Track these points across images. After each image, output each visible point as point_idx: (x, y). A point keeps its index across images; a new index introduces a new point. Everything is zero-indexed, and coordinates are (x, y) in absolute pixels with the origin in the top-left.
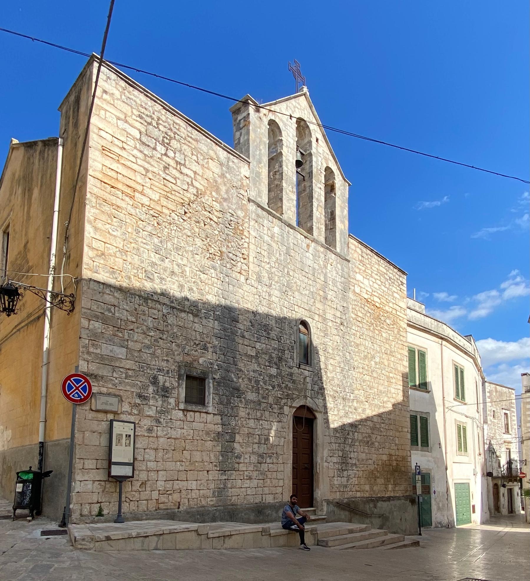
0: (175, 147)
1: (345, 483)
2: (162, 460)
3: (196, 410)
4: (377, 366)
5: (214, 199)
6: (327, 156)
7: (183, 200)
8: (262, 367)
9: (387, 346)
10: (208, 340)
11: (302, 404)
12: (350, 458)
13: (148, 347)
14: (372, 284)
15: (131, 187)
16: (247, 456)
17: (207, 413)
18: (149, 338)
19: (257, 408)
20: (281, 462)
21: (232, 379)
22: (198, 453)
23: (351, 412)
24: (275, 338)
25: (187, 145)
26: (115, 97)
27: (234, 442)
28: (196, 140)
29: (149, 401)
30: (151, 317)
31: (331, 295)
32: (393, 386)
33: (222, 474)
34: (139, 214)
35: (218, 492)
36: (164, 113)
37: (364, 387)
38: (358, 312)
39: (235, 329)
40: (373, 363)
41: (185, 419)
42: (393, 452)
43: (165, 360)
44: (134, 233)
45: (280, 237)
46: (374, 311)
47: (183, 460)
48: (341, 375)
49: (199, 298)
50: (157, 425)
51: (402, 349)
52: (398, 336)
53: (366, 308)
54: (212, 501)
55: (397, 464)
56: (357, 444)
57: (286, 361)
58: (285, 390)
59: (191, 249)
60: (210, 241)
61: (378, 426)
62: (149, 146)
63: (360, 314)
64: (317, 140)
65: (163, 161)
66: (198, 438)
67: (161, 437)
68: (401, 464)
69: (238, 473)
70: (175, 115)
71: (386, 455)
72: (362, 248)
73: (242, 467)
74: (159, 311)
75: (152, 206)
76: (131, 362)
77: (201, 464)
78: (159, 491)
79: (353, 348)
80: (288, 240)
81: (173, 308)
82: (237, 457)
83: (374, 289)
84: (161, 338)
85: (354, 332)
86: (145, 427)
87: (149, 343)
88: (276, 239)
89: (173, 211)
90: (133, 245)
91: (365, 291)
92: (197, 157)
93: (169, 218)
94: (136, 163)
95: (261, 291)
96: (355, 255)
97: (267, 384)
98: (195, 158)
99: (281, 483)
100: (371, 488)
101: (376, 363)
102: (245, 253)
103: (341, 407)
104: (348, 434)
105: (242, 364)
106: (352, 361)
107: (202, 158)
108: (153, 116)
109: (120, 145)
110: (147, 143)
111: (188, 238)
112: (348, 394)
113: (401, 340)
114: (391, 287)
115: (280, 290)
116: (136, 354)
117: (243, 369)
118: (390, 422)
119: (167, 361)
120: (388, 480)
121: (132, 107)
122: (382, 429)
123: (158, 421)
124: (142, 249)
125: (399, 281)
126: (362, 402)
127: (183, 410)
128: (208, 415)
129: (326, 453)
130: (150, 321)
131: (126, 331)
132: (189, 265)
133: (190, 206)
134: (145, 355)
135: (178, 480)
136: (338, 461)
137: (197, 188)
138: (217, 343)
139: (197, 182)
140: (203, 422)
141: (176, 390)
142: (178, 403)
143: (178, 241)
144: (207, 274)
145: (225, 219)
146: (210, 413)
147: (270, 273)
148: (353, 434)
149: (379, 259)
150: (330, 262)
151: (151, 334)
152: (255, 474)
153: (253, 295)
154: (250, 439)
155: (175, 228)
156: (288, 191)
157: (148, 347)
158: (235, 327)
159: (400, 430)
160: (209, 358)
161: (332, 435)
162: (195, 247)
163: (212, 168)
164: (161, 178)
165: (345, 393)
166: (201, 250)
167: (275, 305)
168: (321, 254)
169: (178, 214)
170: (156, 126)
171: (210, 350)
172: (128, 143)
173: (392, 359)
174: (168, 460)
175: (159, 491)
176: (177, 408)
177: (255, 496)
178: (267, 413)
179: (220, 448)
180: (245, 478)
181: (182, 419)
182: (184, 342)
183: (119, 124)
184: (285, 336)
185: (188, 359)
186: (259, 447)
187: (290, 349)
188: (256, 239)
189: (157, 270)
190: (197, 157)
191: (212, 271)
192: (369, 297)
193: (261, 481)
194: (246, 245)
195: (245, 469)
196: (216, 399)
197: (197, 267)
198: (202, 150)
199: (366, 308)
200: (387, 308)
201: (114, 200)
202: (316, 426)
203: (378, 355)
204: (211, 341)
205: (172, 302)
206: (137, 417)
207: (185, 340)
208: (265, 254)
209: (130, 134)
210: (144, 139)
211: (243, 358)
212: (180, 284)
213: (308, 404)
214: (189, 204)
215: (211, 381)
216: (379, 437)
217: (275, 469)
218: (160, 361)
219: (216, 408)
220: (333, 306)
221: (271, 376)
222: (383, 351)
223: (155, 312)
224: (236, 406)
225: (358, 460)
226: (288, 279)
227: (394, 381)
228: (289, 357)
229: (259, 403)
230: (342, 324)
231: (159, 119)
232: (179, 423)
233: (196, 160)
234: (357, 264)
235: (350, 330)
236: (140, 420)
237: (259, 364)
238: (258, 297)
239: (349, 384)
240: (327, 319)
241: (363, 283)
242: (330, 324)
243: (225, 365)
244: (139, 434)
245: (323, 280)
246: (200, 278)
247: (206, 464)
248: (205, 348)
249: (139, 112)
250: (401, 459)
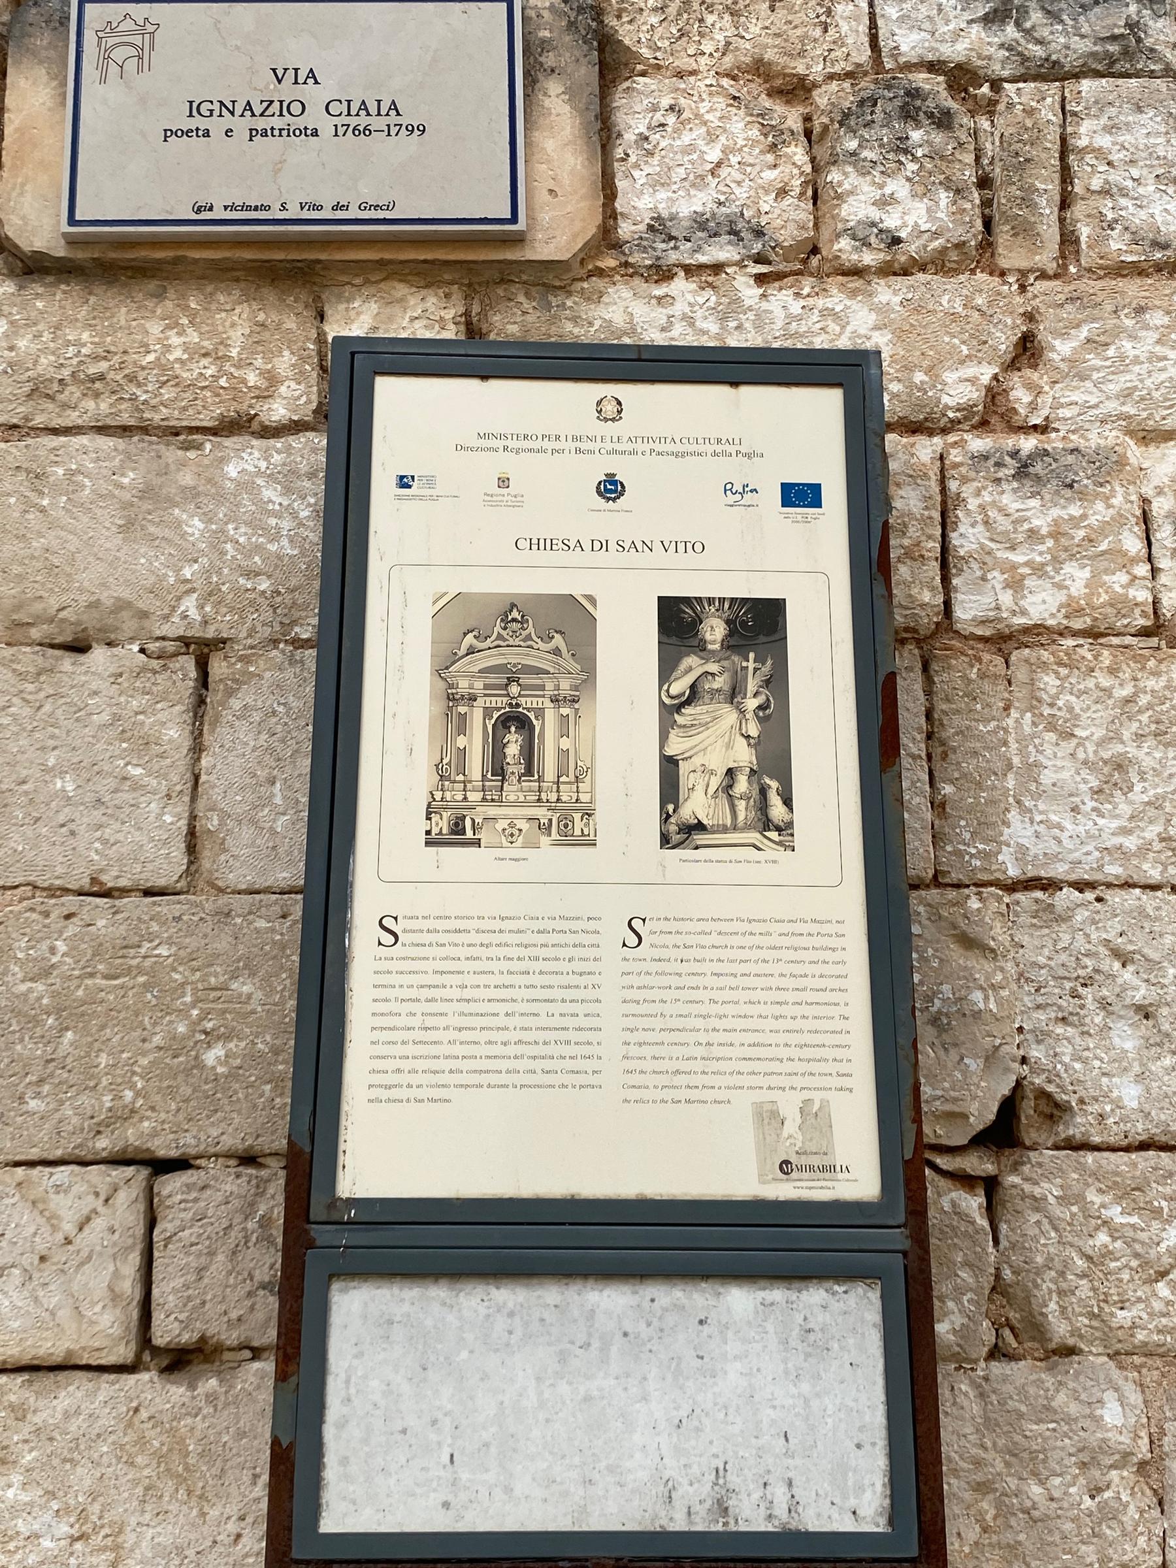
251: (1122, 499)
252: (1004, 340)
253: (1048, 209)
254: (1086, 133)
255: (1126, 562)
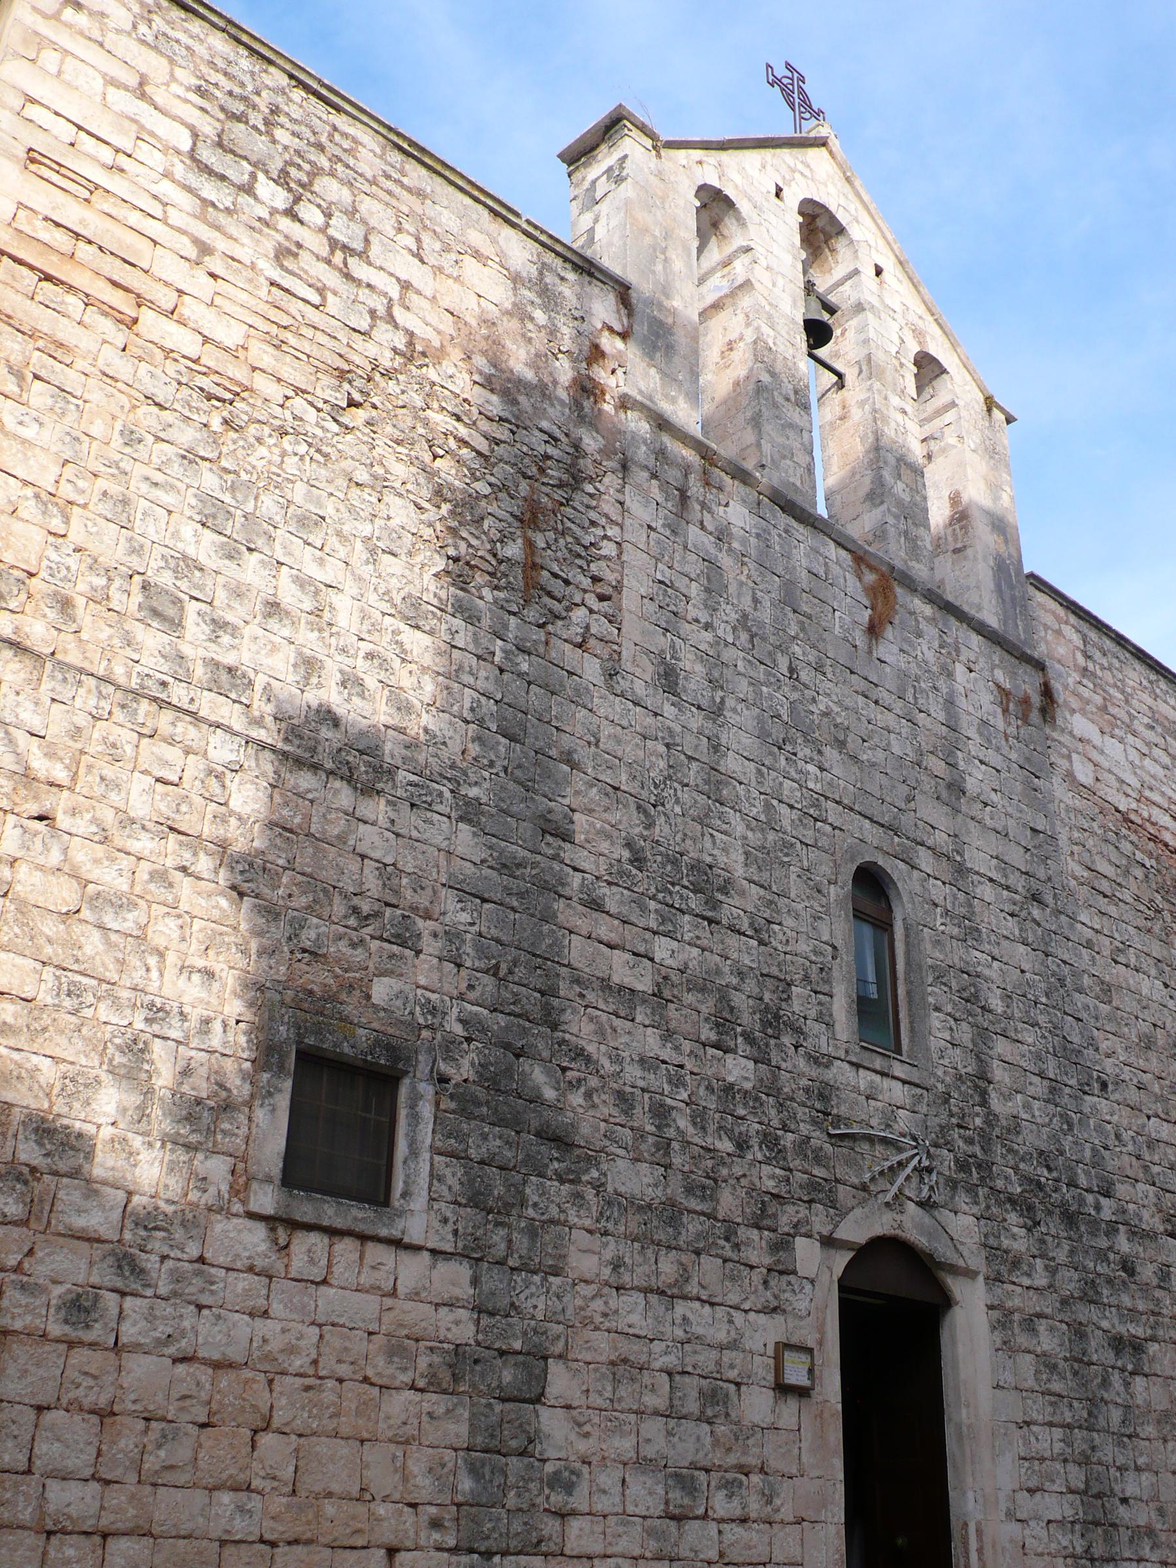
2: (132, 1478)
3: (339, 1223)
6: (920, 323)
8: (687, 1046)
10: (423, 900)
11: (878, 1231)
12: (1124, 1501)
15: (127, 290)
16: (608, 1479)
17: (397, 1244)
18: (126, 862)
19: (660, 1236)
20: (787, 1513)
21: (537, 1088)
22: (345, 1450)
23: (1110, 1281)
24: (745, 926)
25: (380, 200)
26: (112, 25)
27: (538, 1399)
28: (419, 194)
30: (145, 772)
31: (976, 780)
36: (298, 100)
37: (1156, 1169)
39: (556, 866)
41: (280, 1266)
45: (753, 540)
47: (256, 1483)
49: (391, 722)
50: (119, 1284)
53: (1126, 847)
56: (1150, 1430)
57: (799, 1031)
58: (796, 1163)
59: (366, 529)
62: (223, 178)
63: (1103, 867)
64: (879, 272)
65: (277, 231)
66: (344, 1370)
67: (136, 1348)
70: (338, 109)
72: (1085, 627)
74: (187, 752)
76: (19, 960)
77: (360, 1509)
79: (1091, 1002)
80: (787, 556)
83: (1147, 778)
84: (184, 869)
85: (1089, 933)
86: (58, 1290)
87: (123, 885)
89: (300, 391)
90: (101, 484)
92: (418, 240)
93: (278, 411)
94: (164, 221)
95: (678, 729)
96: (1061, 651)
97: (712, 1128)
102: (611, 577)
103: (1062, 1256)
104: (1105, 1383)
106: (1091, 1051)
107: (437, 246)
108: (256, 99)
109: (106, 155)
112: (1090, 1198)
115: (763, 735)
116: (50, 927)
117: (591, 1048)
119: (209, 974)
121: (172, 61)
124: (143, 503)
126: (1151, 1236)
128: (405, 1257)
131: (11, 819)
132: (351, 587)
136: (1069, 1512)
138: (465, 917)
140: (374, 1289)
141: (242, 1118)
142: (247, 1185)
143: (308, 497)
145: (525, 449)
146: (417, 1248)
147: (712, 660)
148: (1127, 1385)
149: (1153, 677)
153: (638, 740)
155: (302, 448)
158: (555, 857)
160: (422, 981)
161: (1031, 1383)
162: (386, 528)
164: (262, 279)
166: (408, 539)
167: (741, 789)
168: (923, 625)
169: (320, 405)
170: (263, 128)
171: (430, 946)
174: (168, 1477)
176: (237, 1207)
178: (710, 1264)
179: (464, 1429)
181: (259, 1263)
182: (303, 901)
183: (108, 97)
184: (789, 922)
185: (318, 978)
186: (670, 1433)
187: (814, 976)
189: (201, 588)
190: (418, 240)
192: (1134, 805)
194: (609, 549)
196: (450, 1180)
198: (440, 225)
199: (1126, 847)
201: (44, 320)
202: (954, 1342)
206: (16, 1232)
208: (694, 590)
210: (207, 155)
211: (591, 997)
212: (300, 654)
215: (427, 1090)
218: (170, 972)
219: (445, 1221)
223: (173, 754)
224: (552, 1221)
229: (672, 1213)
230: (1036, 898)
231: (275, 110)
232: (244, 1282)
233: (415, 249)
235: (1072, 927)
236: (31, 1252)
237: (668, 1035)
238: (662, 749)
240: (969, 870)
241: (1102, 752)
242: (986, 892)
243: (502, 1020)
244: (18, 1325)
245: (942, 717)
247: (381, 1510)
248: (405, 939)
249: (199, 78)
251: (44, 1298)
252: (26, 1250)
253: (46, 1215)
254: (61, 1194)
255: (40, 1315)
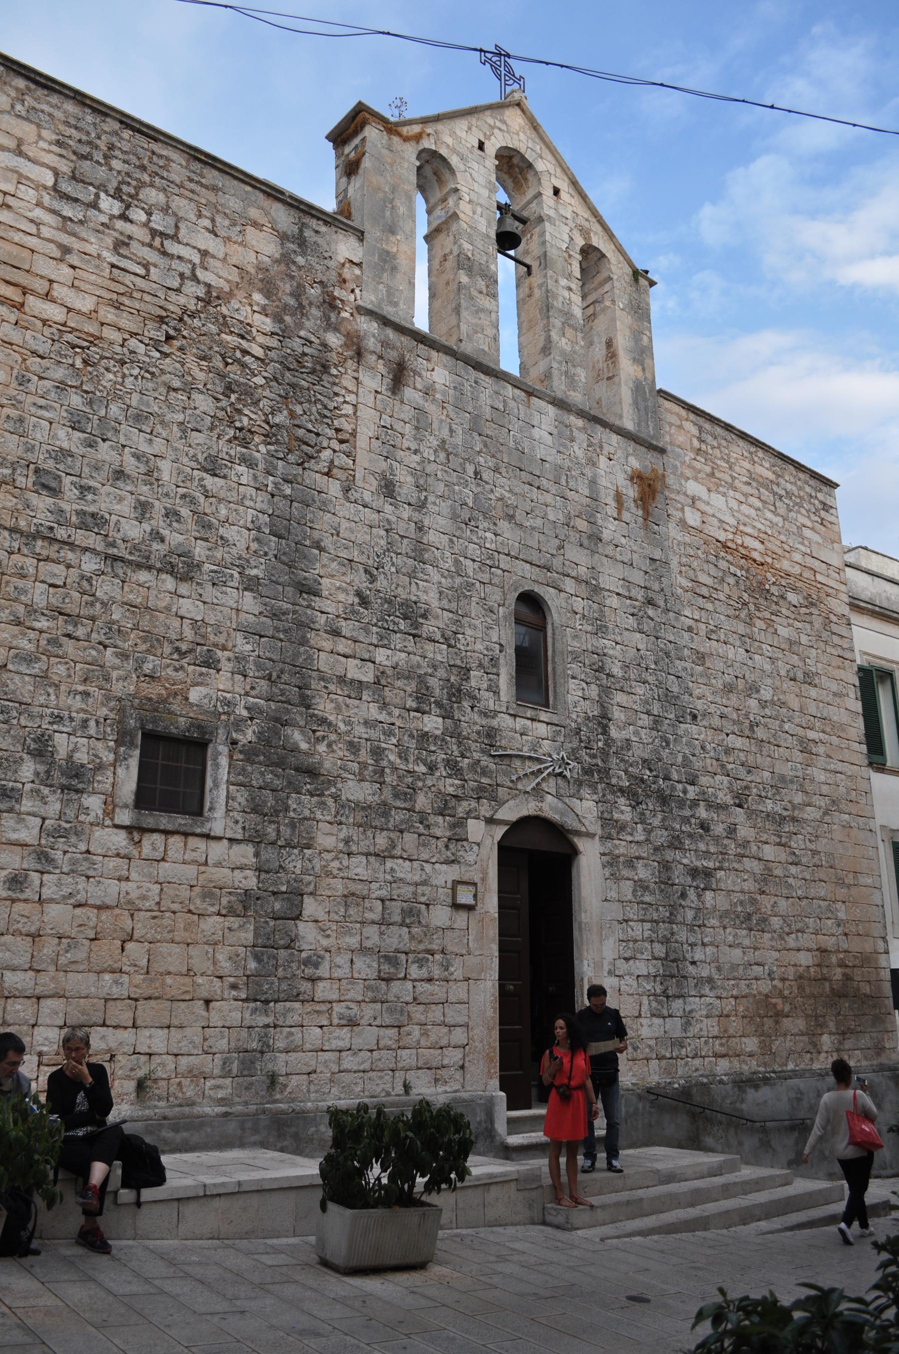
0: (150, 202)
1: (678, 1033)
3: (170, 827)
4: (768, 712)
5: (255, 308)
6: (586, 224)
7: (165, 310)
8: (396, 712)
9: (795, 659)
10: (221, 640)
12: (693, 963)
13: (29, 659)
14: (736, 508)
18: (32, 635)
22: (176, 949)
24: (438, 637)
27: (298, 917)
28: (214, 189)
29: (18, 801)
30: (43, 582)
32: (821, 761)
33: (254, 1011)
34: (31, 341)
35: (242, 1062)
38: (699, 573)
39: (309, 612)
40: (753, 703)
42: (830, 943)
43: (76, 693)
44: (14, 384)
46: (747, 571)
48: (654, 733)
50: (39, 867)
51: (839, 667)
52: (825, 635)
53: (723, 564)
54: (218, 1087)
55: (844, 975)
56: (714, 922)
57: (474, 698)
59: (180, 417)
60: (238, 399)
61: (778, 872)
62: (76, 200)
63: (704, 578)
64: (556, 192)
66: (175, 907)
67: (51, 901)
68: (857, 974)
69: (309, 1007)
71: (809, 950)
73: (323, 990)
74: (69, 566)
75: (73, 325)
77: (187, 980)
78: (40, 1054)
79: (688, 665)
81: (116, 559)
82: (307, 962)
83: (742, 518)
84: (69, 636)
87: (31, 647)
88: (438, 396)
89: (133, 334)
91: (715, 522)
93: (118, 349)
94: (38, 236)
96: (681, 439)
97: (411, 759)
98: (207, 223)
99: (459, 1036)
100: (766, 1049)
101: (763, 704)
102: (348, 427)
105: (330, 706)
106: (686, 696)
107: (227, 222)
108: (98, 142)
110: (74, 195)
111: (173, 394)
113: (835, 646)
114: (792, 514)
117: (332, 718)
118: (816, 860)
120: (817, 1025)
121: (39, 126)
122: (790, 880)
123: (43, 856)
125: (816, 502)
127: (129, 829)
129: (610, 950)
130: (38, 592)
132: (171, 455)
133: (185, 324)
134: (17, 678)
135: (104, 1025)
137: (209, 286)
138: (249, 647)
139: (207, 273)
140: (194, 862)
141: (110, 774)
142: (113, 811)
144: (225, 477)
145: (289, 351)
146: (219, 839)
148: (699, 896)
149: (753, 449)
150: (605, 452)
151: (37, 625)
152: (369, 1010)
153: (366, 529)
154: (351, 911)
155: (136, 371)
156: (475, 293)
157: (29, 659)
158: (309, 606)
159: (850, 880)
160: (221, 687)
163: (254, 243)
164: (105, 264)
165: (668, 783)
168: (576, 433)
170: (103, 161)
171: (226, 666)
172: (20, 195)
173: (813, 692)
175: (40, 1054)
176: (108, 822)
177: (371, 1074)
178: (409, 838)
180: (336, 1021)
181: (123, 852)
184: (469, 632)
185: (154, 691)
186: (382, 933)
188: (379, 396)
190: (213, 221)
191: (242, 469)
192: (731, 537)
193: (393, 1032)
195: (335, 997)
197: (194, 458)
198: (229, 208)
200: (785, 565)
203: (769, 681)
204: (230, 645)
205: (113, 545)
207: (145, 640)
208: (408, 429)
209: (28, 178)
210: (66, 187)
211: (332, 687)
212: (138, 500)
213: (548, 813)
214: (181, 320)
215: (224, 749)
216: (783, 904)
217: (442, 996)
218: (62, 697)
220: (619, 557)
221: (424, 736)
222: (783, 673)
224: (305, 819)
225: (719, 969)
226: (477, 490)
227: (821, 749)
228: (485, 686)
229: (384, 809)
230: (650, 602)
231: (111, 147)
232: (112, 863)
234: (687, 459)
237: (384, 706)
238: (383, 533)
239: (680, 759)
242: (614, 601)
243: (273, 705)
245: (586, 492)
246: (203, 486)
247: (200, 980)
248: (210, 663)
249: (57, 134)
250: (857, 962)
